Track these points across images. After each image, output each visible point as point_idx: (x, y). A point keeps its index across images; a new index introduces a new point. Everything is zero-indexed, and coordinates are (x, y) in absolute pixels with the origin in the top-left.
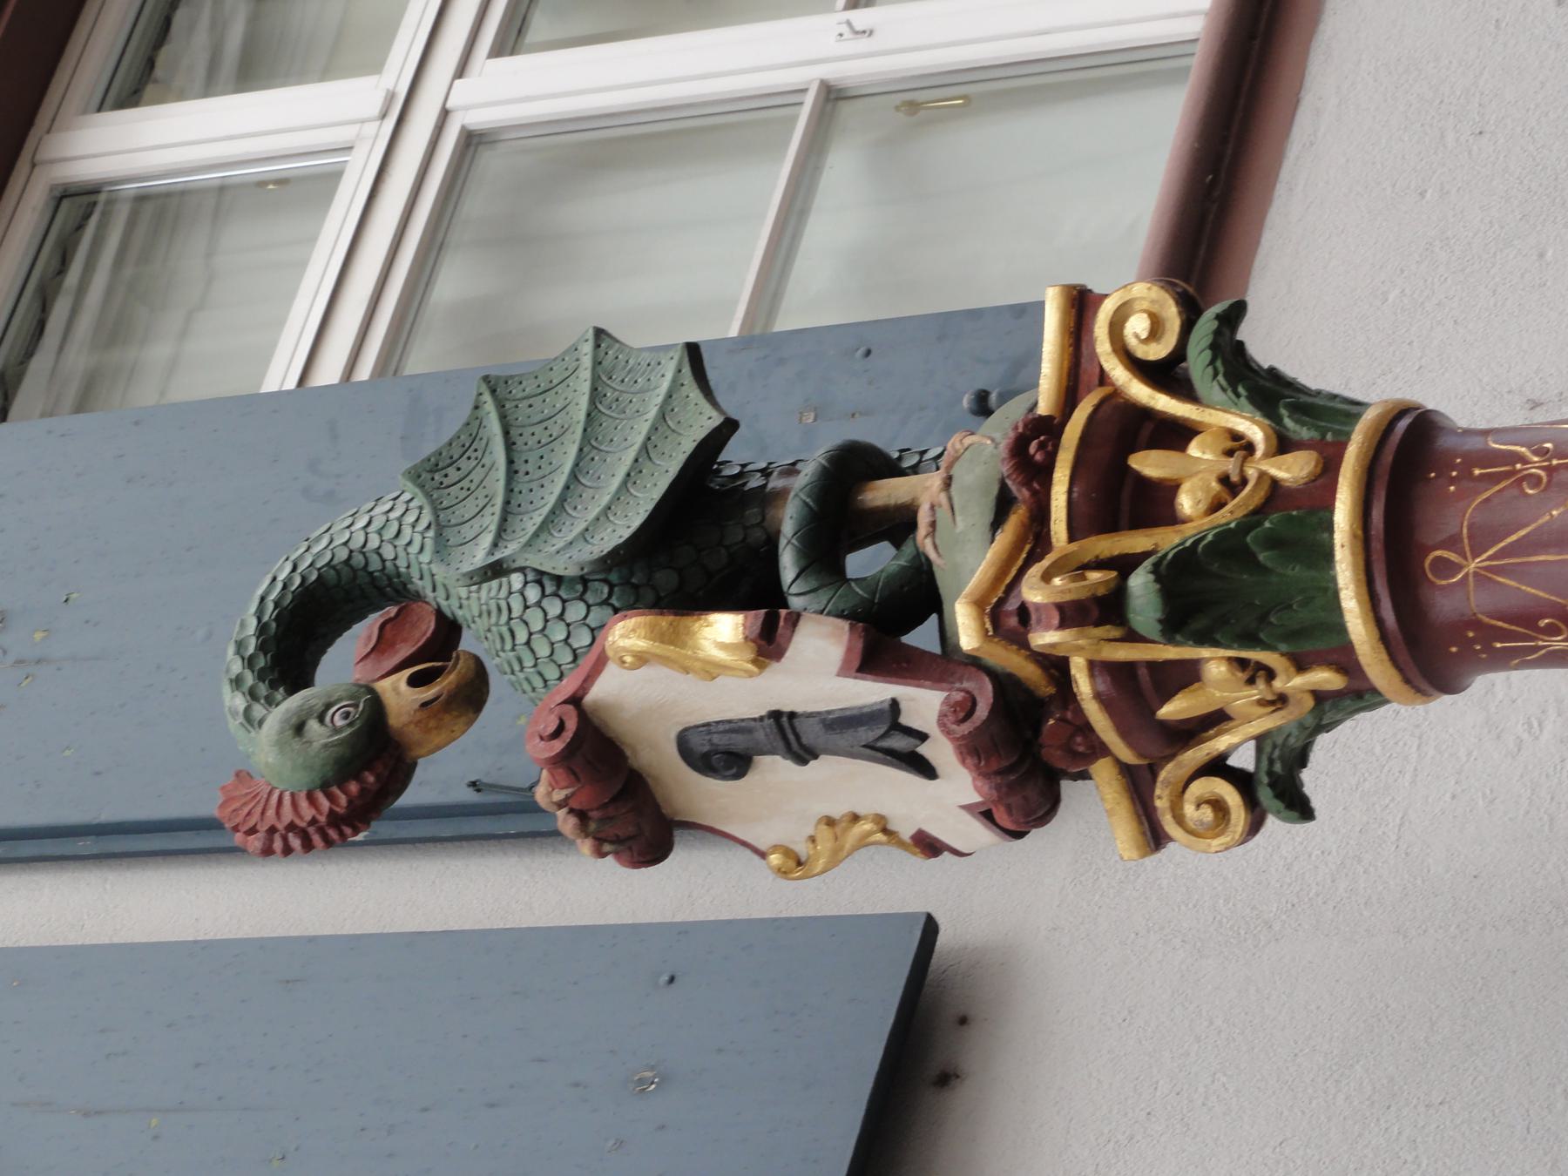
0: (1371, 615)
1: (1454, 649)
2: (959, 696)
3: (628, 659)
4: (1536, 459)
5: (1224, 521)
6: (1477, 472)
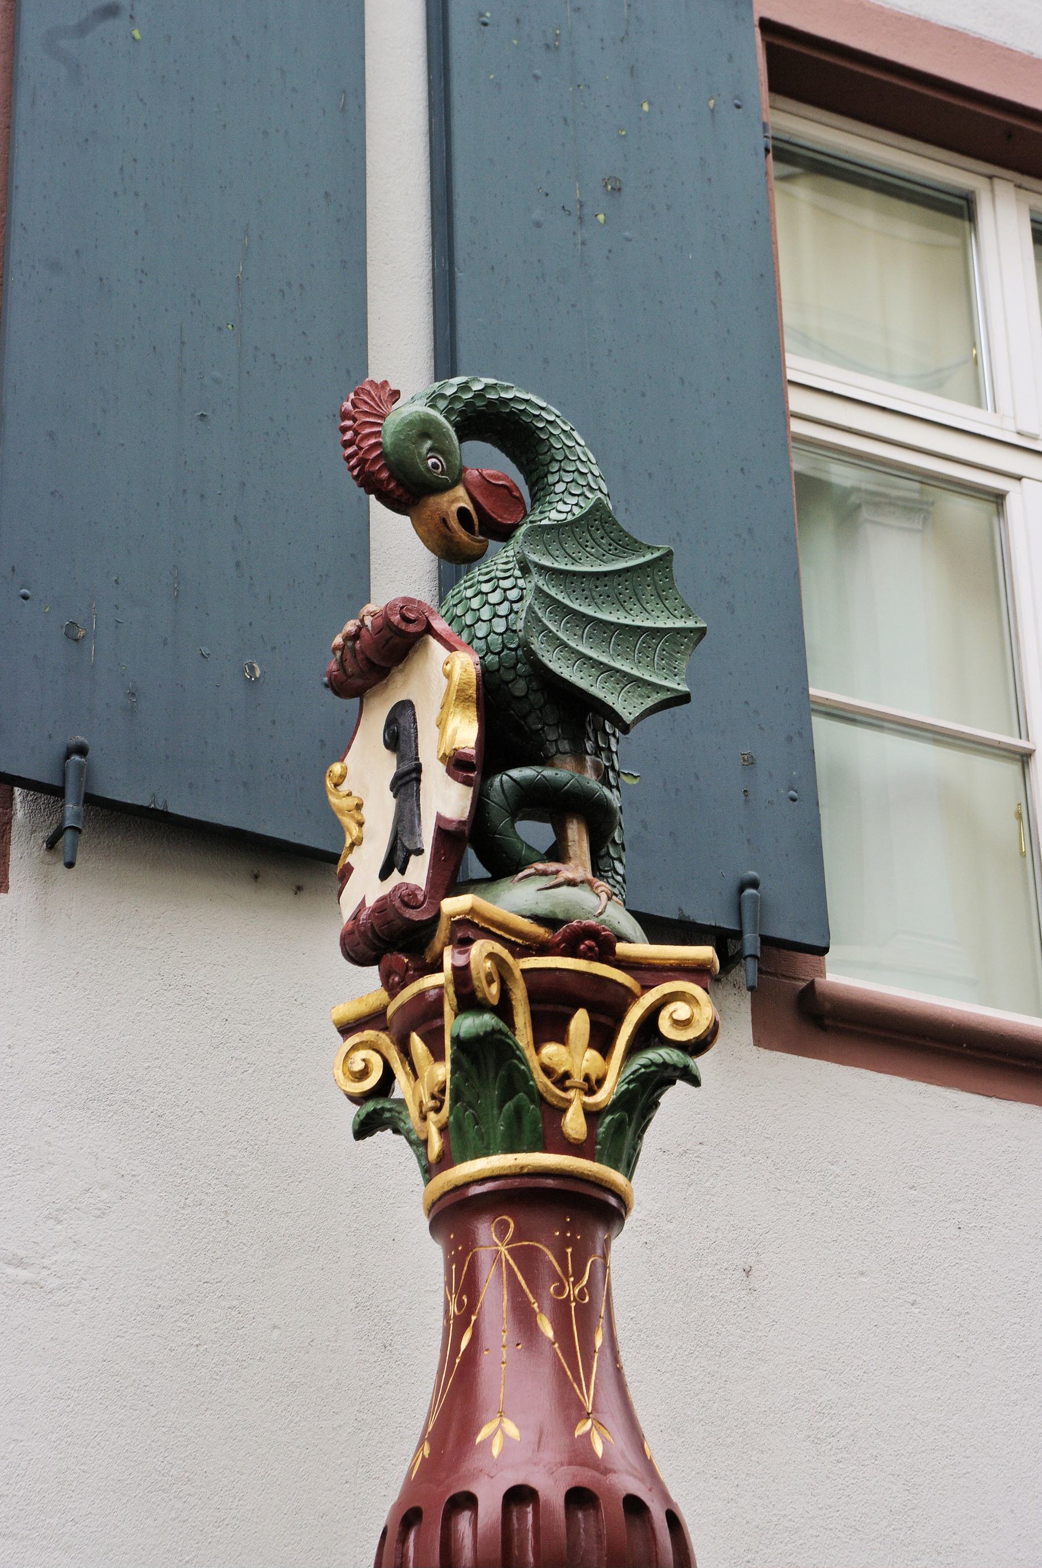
0: (471, 1179)
1: (452, 1236)
2: (421, 898)
3: (448, 667)
4: (576, 1292)
5: (535, 1076)
6: (569, 1250)
